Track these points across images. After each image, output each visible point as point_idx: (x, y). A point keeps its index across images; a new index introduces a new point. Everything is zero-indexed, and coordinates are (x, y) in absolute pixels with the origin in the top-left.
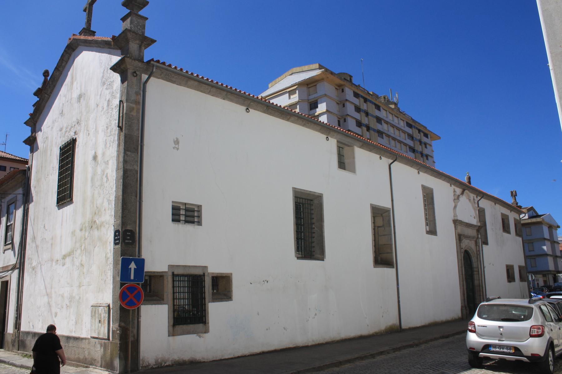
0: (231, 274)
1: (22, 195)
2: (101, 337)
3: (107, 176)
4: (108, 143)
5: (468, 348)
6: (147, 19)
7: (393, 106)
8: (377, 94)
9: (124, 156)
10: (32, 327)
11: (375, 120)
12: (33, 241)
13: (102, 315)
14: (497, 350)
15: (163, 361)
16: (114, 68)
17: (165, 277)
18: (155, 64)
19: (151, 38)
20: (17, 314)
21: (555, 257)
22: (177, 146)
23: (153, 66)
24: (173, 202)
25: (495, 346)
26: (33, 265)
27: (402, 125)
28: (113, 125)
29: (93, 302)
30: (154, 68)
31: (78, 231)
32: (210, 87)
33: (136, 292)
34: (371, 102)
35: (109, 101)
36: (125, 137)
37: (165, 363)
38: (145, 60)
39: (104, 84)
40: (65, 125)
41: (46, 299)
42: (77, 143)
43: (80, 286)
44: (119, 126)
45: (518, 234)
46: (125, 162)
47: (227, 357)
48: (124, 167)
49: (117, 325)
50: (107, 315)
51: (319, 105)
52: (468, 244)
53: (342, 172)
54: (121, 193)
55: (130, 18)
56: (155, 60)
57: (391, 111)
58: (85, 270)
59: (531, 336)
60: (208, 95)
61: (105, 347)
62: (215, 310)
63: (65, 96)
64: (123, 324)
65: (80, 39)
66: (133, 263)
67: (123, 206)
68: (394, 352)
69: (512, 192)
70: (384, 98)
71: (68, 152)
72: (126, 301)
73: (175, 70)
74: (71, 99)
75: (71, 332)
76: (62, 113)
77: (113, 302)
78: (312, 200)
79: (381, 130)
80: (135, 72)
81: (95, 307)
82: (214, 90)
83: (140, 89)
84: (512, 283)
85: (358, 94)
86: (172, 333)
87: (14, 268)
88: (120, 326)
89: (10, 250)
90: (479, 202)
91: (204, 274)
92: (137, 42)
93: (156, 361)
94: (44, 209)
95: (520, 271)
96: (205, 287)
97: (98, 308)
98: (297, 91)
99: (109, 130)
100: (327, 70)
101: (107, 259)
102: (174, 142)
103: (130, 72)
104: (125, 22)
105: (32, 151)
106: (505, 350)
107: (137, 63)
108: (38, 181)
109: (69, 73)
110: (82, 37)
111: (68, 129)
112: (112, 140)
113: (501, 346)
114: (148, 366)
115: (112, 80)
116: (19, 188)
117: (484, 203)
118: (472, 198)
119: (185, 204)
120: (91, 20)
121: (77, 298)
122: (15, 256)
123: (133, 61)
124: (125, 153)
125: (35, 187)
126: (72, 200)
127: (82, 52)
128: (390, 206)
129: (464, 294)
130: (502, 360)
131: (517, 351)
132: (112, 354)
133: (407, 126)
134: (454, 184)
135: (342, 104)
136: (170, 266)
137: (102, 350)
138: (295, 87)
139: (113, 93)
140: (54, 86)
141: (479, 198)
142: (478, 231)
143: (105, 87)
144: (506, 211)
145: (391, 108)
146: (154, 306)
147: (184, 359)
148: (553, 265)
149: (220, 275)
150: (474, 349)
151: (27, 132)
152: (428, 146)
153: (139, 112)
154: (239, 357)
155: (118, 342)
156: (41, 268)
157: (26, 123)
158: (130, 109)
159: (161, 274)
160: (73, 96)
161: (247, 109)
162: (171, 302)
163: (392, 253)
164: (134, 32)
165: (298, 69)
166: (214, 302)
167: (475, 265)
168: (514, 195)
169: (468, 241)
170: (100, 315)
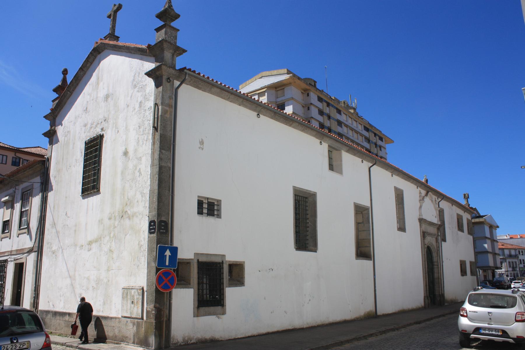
0: (244, 262)
1: (40, 184)
2: (134, 316)
3: (139, 171)
4: (141, 141)
5: (460, 330)
6: (179, 30)
7: (352, 111)
8: (338, 99)
10: (52, 306)
11: (336, 123)
12: (52, 227)
13: (135, 297)
14: (487, 332)
16: (149, 74)
17: (192, 264)
18: (188, 72)
20: (35, 294)
21: (495, 254)
23: (186, 73)
24: (199, 197)
25: (485, 329)
26: (53, 249)
27: (360, 128)
28: (146, 125)
29: (125, 285)
30: (185, 75)
33: (170, 277)
34: (333, 106)
35: (141, 102)
36: (161, 137)
38: (177, 68)
39: (135, 86)
40: (90, 122)
41: (68, 281)
42: (104, 139)
43: (108, 270)
44: (154, 127)
45: (470, 233)
46: (160, 159)
47: (239, 337)
49: (152, 306)
51: (286, 108)
52: (430, 240)
53: (331, 173)
54: (156, 187)
55: (164, 29)
56: (192, 70)
57: (350, 116)
58: (115, 256)
59: (517, 321)
61: (138, 326)
62: (231, 294)
63: (90, 95)
64: (157, 305)
65: (109, 44)
67: (158, 199)
68: (381, 334)
69: (465, 195)
70: (344, 103)
71: (94, 148)
74: (97, 98)
76: (86, 110)
77: (147, 285)
78: (307, 198)
79: (342, 132)
80: (169, 78)
82: (232, 97)
83: (173, 94)
84: (465, 277)
85: (322, 99)
87: (30, 251)
88: (155, 307)
89: (26, 235)
90: (440, 203)
92: (171, 51)
94: (66, 197)
95: (471, 266)
96: (223, 273)
97: (129, 291)
98: (266, 94)
99: (141, 130)
100: (294, 75)
101: (140, 246)
102: (200, 143)
103: (165, 78)
104: (159, 33)
105: (51, 143)
106: (494, 333)
107: (172, 71)
108: (59, 171)
109: (95, 74)
110: (107, 41)
111: (94, 126)
112: (145, 138)
113: (490, 329)
114: (177, 343)
116: (36, 176)
117: (444, 204)
118: (434, 200)
119: (208, 198)
121: (105, 280)
122: (31, 239)
123: (168, 69)
124: (160, 151)
125: (55, 177)
126: (99, 190)
127: (109, 55)
128: (369, 205)
129: (426, 286)
130: (490, 341)
131: (504, 333)
132: (146, 332)
133: (365, 129)
134: (420, 187)
135: (307, 107)
136: (196, 254)
137: (135, 328)
138: (264, 90)
139: (146, 95)
140: (77, 85)
141: (440, 199)
142: (438, 229)
143: (136, 89)
144: (461, 212)
145: (350, 113)
146: (182, 289)
148: (493, 262)
150: (466, 331)
151: (46, 126)
152: (382, 149)
153: (172, 115)
154: (249, 337)
155: (153, 321)
158: (165, 112)
159: (188, 261)
161: (258, 114)
162: (196, 286)
163: (370, 247)
164: (169, 42)
165: (267, 73)
167: (435, 259)
168: (466, 197)
169: (430, 238)
170: (133, 296)
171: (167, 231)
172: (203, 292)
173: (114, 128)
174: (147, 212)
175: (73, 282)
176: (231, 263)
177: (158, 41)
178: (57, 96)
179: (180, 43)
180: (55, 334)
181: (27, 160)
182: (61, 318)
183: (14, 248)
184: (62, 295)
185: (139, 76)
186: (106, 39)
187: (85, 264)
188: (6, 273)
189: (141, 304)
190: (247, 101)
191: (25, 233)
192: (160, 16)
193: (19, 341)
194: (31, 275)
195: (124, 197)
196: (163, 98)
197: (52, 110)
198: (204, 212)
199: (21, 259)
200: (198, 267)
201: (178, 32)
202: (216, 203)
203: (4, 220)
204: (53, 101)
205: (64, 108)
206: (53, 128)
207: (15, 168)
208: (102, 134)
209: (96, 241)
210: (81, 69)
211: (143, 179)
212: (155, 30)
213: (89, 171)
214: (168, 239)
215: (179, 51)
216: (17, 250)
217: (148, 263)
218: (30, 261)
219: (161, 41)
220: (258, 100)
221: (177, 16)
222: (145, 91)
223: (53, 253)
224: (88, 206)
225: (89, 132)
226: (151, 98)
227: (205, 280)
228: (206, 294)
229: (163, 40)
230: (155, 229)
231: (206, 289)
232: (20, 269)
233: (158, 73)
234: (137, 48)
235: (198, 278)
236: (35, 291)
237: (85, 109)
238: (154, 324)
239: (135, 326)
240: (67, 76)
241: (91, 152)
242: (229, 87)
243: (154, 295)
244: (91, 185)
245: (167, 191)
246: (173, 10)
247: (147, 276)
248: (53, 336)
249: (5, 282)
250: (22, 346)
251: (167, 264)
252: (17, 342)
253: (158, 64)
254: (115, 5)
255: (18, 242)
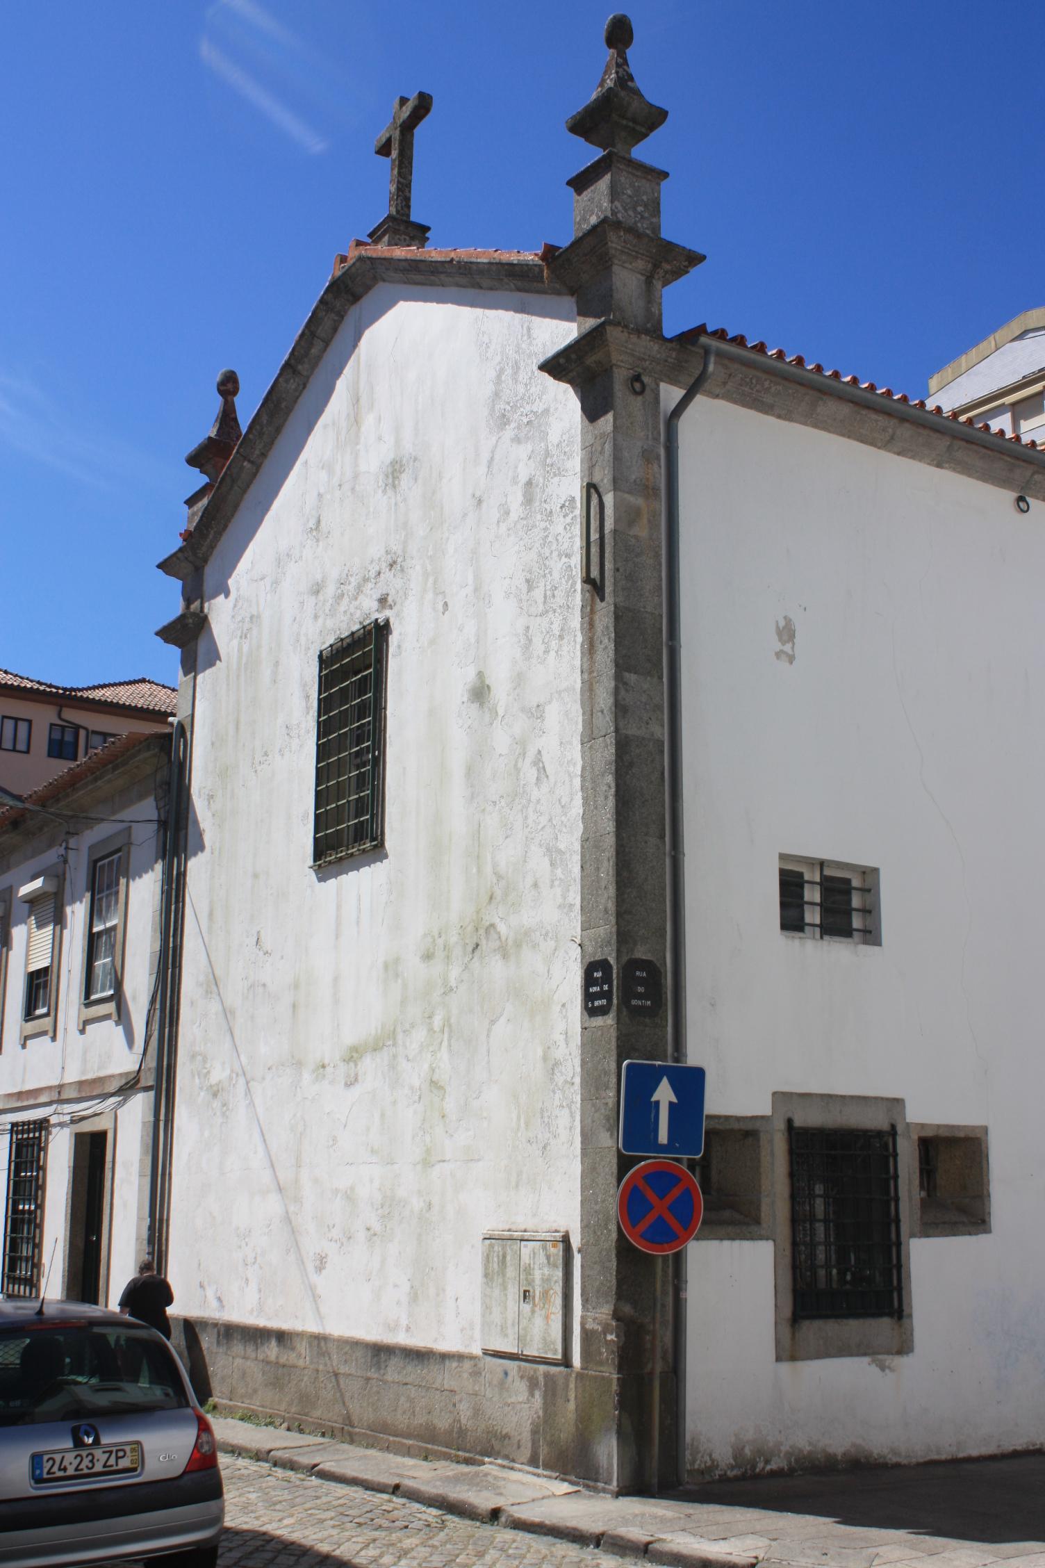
1: (154, 826)
2: (531, 1351)
3: (538, 761)
4: (537, 641)
9: (617, 689)
10: (215, 1304)
13: (537, 1275)
15: (759, 1452)
16: (556, 367)
17: (763, 1138)
18: (714, 343)
19: (688, 246)
20: (151, 1253)
22: (787, 648)
23: (707, 351)
24: (783, 857)
28: (556, 575)
29: (495, 1223)
30: (703, 358)
31: (413, 966)
32: (893, 422)
33: (676, 1192)
35: (529, 483)
36: (617, 618)
37: (767, 1462)
38: (670, 330)
40: (334, 574)
41: (273, 1205)
42: (393, 640)
43: (427, 1163)
44: (588, 580)
46: (621, 709)
47: (975, 1453)
48: (617, 730)
50: (559, 1274)
54: (609, 826)
55: (608, 177)
56: (730, 335)
58: (450, 1105)
60: (882, 453)
61: (551, 1391)
62: (935, 1266)
63: (328, 467)
64: (627, 1309)
66: (665, 1082)
71: (354, 677)
72: (643, 1225)
73: (779, 365)
74: (356, 476)
75: (393, 1328)
76: (316, 528)
77: (585, 1227)
80: (637, 378)
81: (502, 1243)
82: (906, 431)
83: (656, 439)
86: (789, 1351)
87: (129, 1086)
88: (616, 1315)
89: (110, 1024)
91: (893, 1127)
93: (738, 1453)
94: (255, 876)
97: (511, 1248)
99: (538, 594)
101: (553, 1067)
102: (780, 633)
103: (620, 376)
104: (587, 194)
105: (191, 665)
107: (645, 345)
108: (224, 773)
109: (341, 385)
110: (382, 250)
111: (350, 588)
115: (539, 407)
116: (141, 797)
119: (822, 864)
120: (409, 186)
121: (417, 1204)
123: (634, 338)
124: (618, 677)
126: (381, 845)
132: (584, 1418)
139: (547, 454)
140: (278, 430)
143: (509, 432)
146: (726, 1243)
147: (831, 1450)
149: (962, 1135)
151: (168, 599)
154: (1015, 1454)
155: (612, 1374)
156: (248, 1091)
157: (165, 566)
158: (628, 516)
159: (749, 1126)
160: (363, 467)
161: (1021, 499)
164: (631, 230)
166: (927, 1235)
170: (528, 1270)
171: (659, 1002)
172: (812, 1256)
173: (430, 595)
174: (573, 925)
175: (292, 1209)
176: (929, 1133)
177: (586, 227)
178: (204, 480)
179: (672, 230)
180: (230, 1412)
181: (105, 735)
182: (250, 1350)
183: (72, 1076)
184: (250, 1260)
185: (516, 381)
186: (376, 242)
187: (335, 1139)
188: (42, 1169)
189: (558, 1301)
190: (966, 443)
191: (107, 1017)
192: (586, 125)
193: (105, 1440)
194: (135, 1178)
195: (479, 871)
196: (617, 458)
197: (188, 536)
198: (808, 919)
199: (99, 1113)
200: (791, 1152)
201: (664, 184)
202: (856, 883)
203: (32, 968)
204: (190, 502)
205: (231, 527)
206: (195, 606)
207: (61, 767)
208: (381, 618)
209: (376, 1046)
210: (290, 368)
211: (552, 792)
212: (569, 183)
213: (340, 767)
214: (665, 1037)
215: (674, 261)
216: (81, 1084)
217: (584, 1135)
218: (130, 1125)
219: (595, 228)
220: (1018, 438)
221: (657, 117)
222: (544, 436)
223: (215, 1095)
224: (339, 907)
225: (332, 613)
226: (569, 464)
227: (819, 1205)
228: (827, 1266)
229: (604, 221)
230: (607, 995)
231: (827, 1244)
232: (93, 1153)
233: (590, 360)
234: (500, 264)
235: (793, 1197)
236: (151, 1241)
237: (312, 524)
238: (615, 1387)
239: (537, 1394)
240: (237, 400)
241: (344, 695)
242: (889, 393)
243: (614, 1264)
244: (348, 824)
245: (653, 841)
246: (637, 92)
247: (584, 1188)
248: (221, 1420)
249: (40, 1206)
250: (112, 1461)
251: (663, 1137)
252: (97, 1442)
253: (591, 323)
254: (403, 101)
255: (85, 1053)
